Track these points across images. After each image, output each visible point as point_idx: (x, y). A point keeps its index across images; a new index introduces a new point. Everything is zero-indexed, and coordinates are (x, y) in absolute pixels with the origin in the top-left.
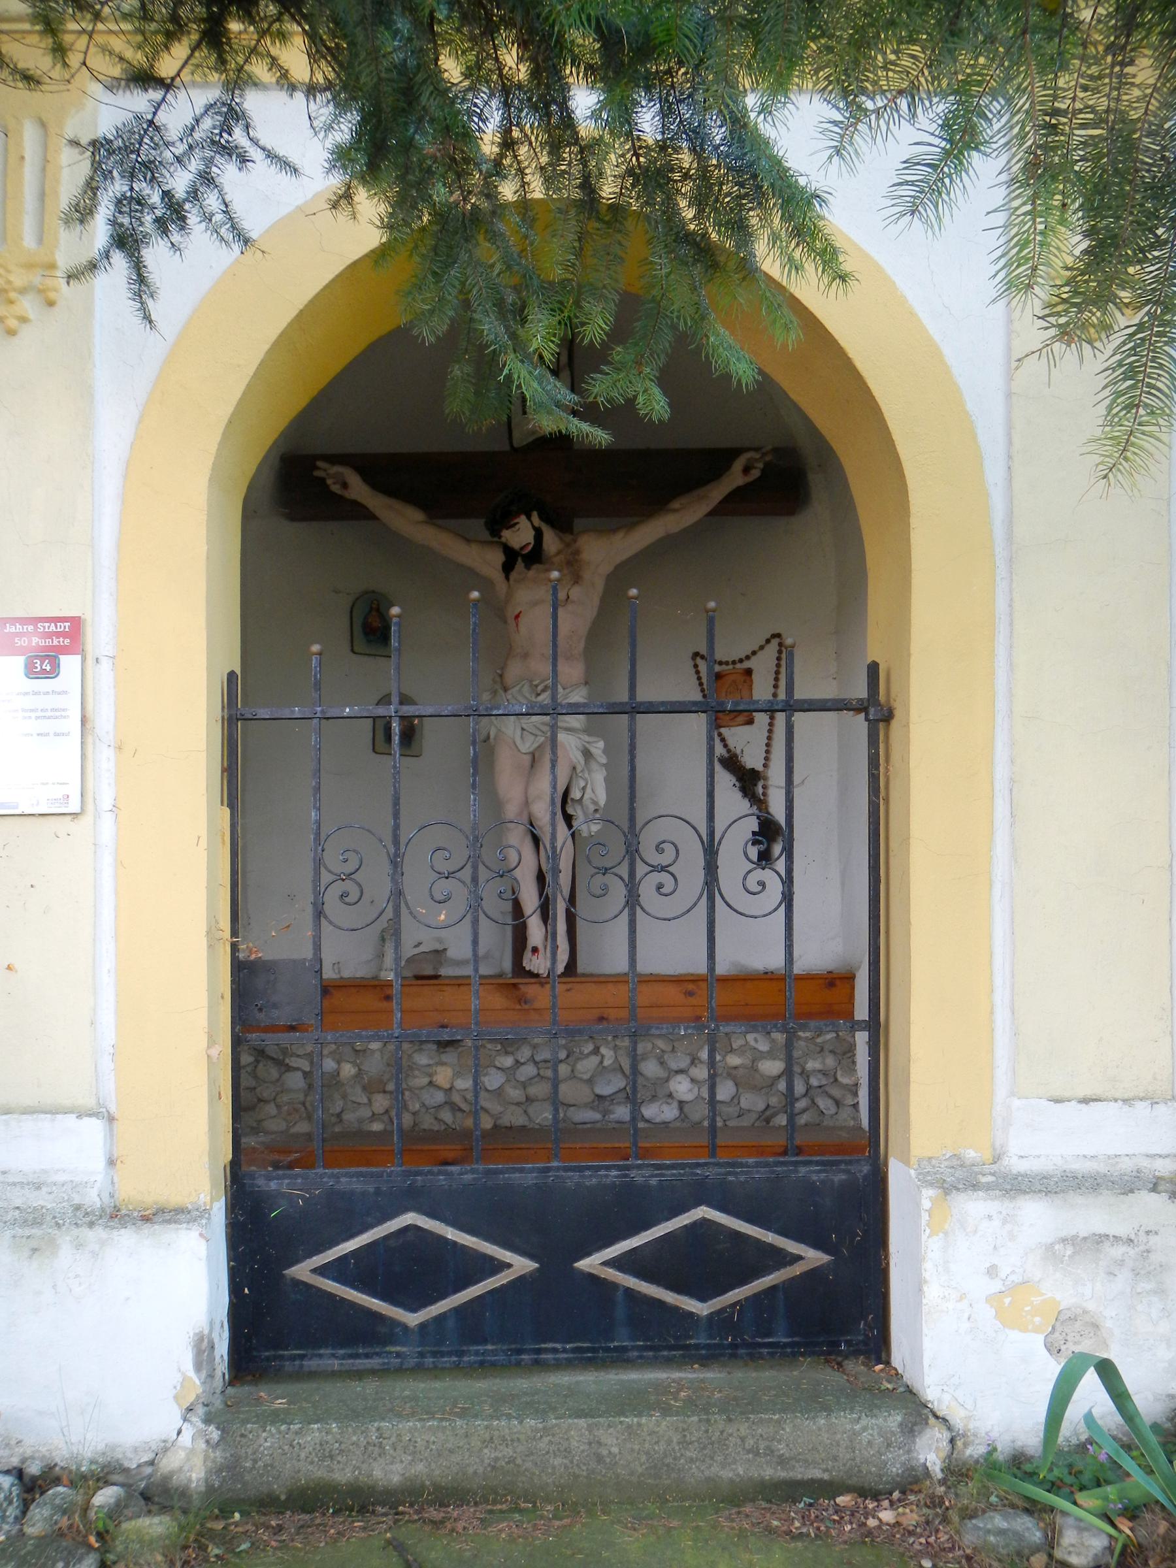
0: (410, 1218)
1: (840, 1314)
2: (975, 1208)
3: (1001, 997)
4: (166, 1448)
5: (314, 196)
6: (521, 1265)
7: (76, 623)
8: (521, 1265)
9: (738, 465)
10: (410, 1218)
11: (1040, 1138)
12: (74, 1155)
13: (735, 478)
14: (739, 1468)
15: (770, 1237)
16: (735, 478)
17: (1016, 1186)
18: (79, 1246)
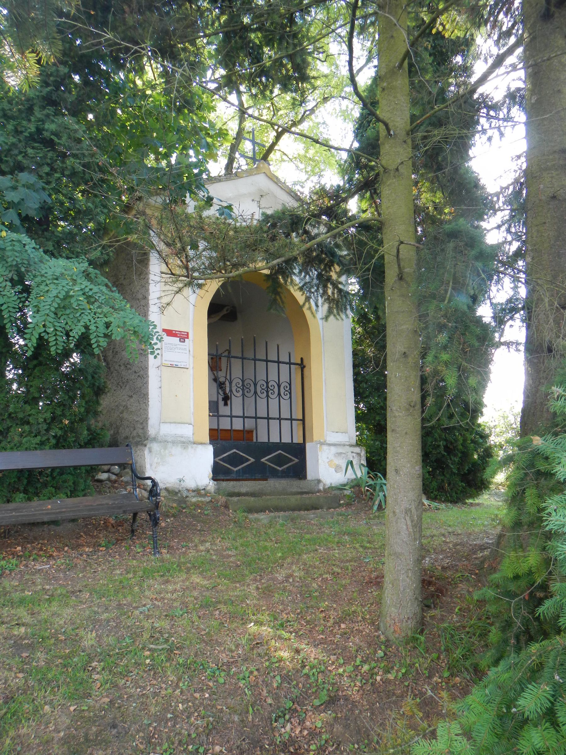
0: (234, 450)
1: (299, 471)
2: (325, 447)
3: (325, 415)
4: (207, 486)
5: (523, 418)
6: (252, 460)
7: (188, 333)
8: (252, 460)
9: (225, 309)
10: (234, 450)
11: (332, 438)
12: (187, 431)
13: (224, 312)
14: (295, 490)
15: (290, 456)
16: (224, 312)
17: (330, 445)
18: (192, 447)
